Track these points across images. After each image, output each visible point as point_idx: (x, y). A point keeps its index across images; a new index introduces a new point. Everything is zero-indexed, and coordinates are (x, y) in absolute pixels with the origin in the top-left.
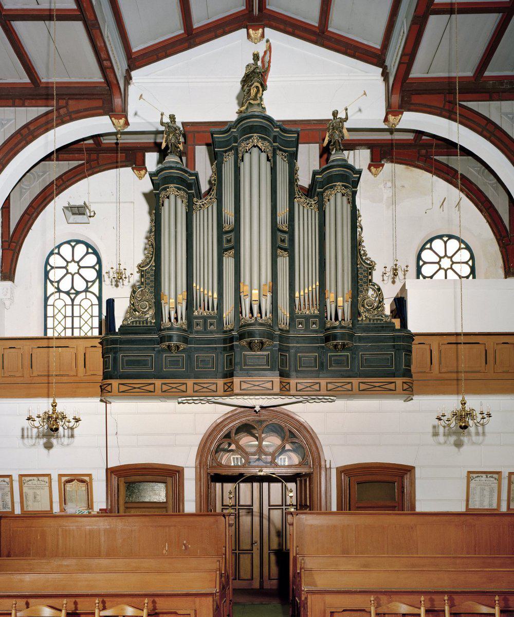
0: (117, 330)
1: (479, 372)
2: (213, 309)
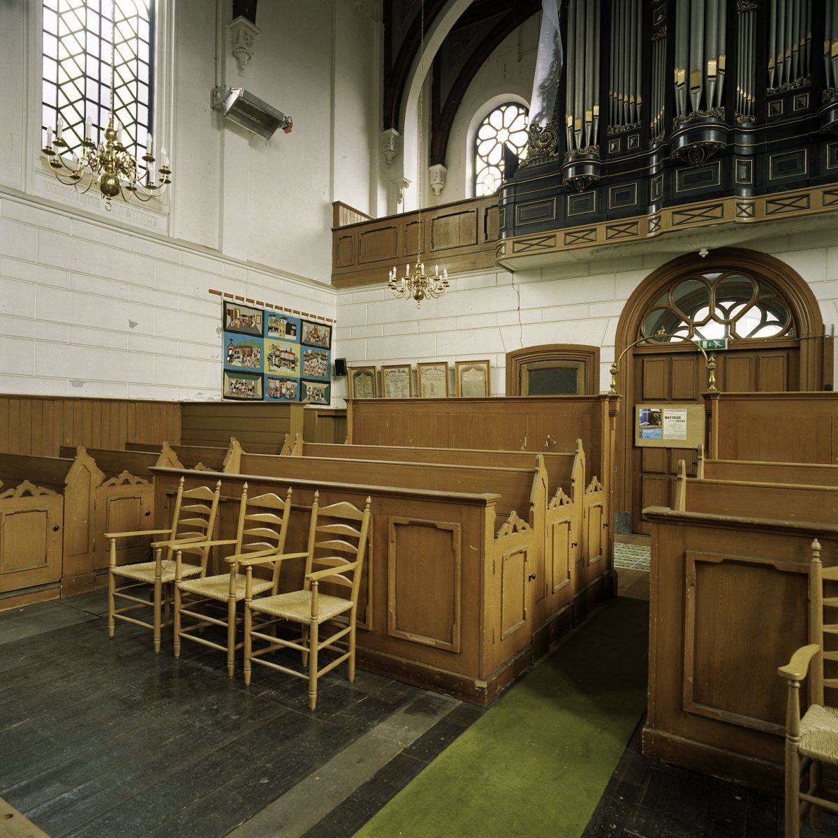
2: (635, 120)
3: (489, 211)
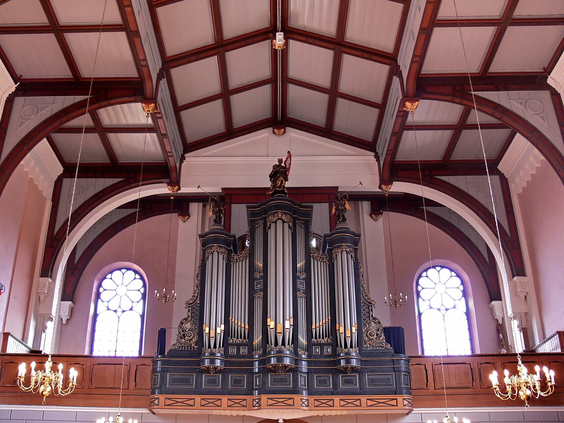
0: (166, 354)
1: (468, 388)
2: (245, 338)
3: (138, 367)
